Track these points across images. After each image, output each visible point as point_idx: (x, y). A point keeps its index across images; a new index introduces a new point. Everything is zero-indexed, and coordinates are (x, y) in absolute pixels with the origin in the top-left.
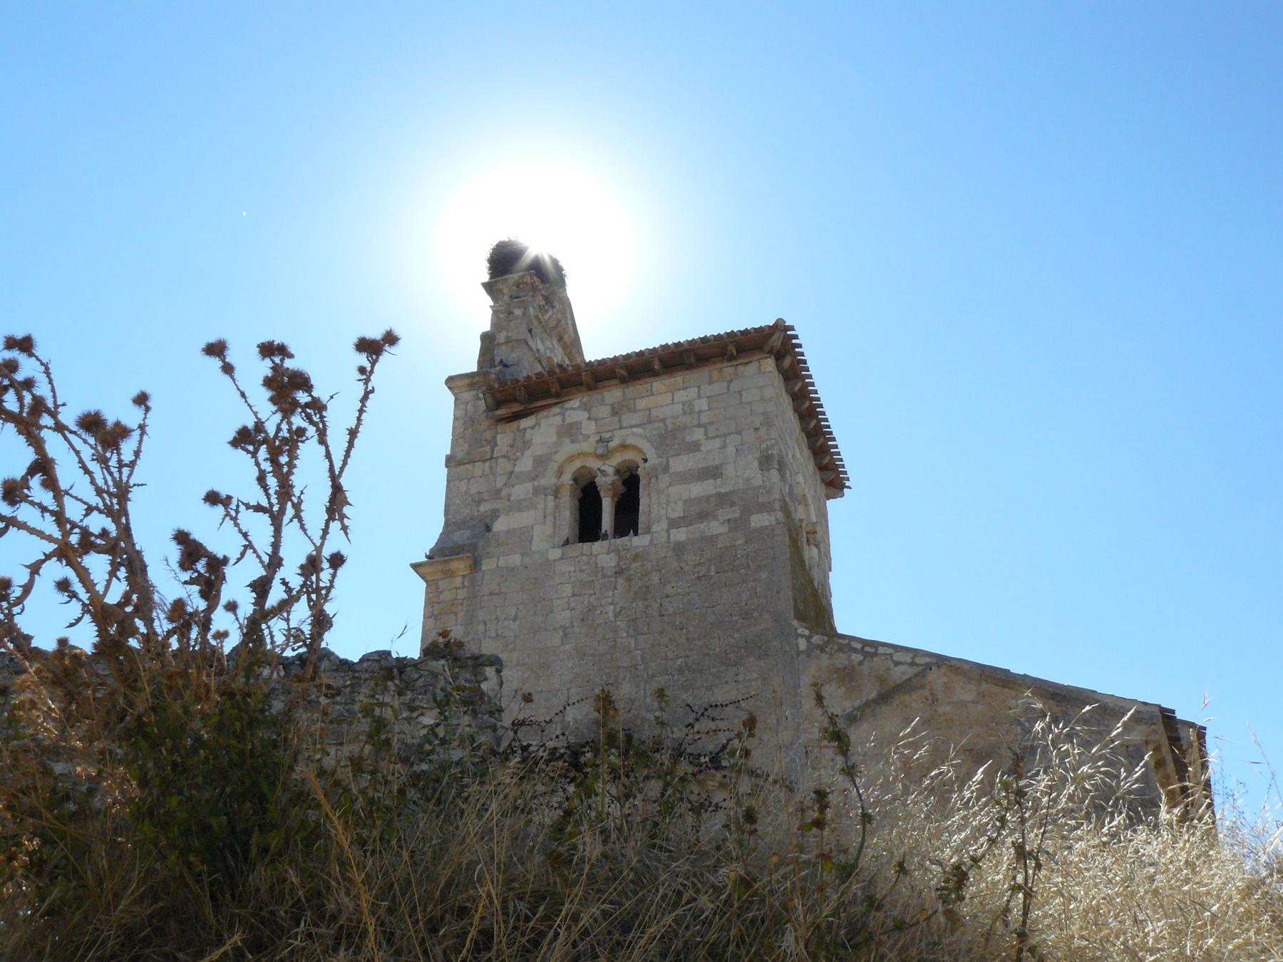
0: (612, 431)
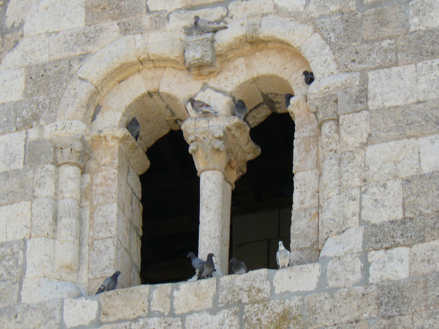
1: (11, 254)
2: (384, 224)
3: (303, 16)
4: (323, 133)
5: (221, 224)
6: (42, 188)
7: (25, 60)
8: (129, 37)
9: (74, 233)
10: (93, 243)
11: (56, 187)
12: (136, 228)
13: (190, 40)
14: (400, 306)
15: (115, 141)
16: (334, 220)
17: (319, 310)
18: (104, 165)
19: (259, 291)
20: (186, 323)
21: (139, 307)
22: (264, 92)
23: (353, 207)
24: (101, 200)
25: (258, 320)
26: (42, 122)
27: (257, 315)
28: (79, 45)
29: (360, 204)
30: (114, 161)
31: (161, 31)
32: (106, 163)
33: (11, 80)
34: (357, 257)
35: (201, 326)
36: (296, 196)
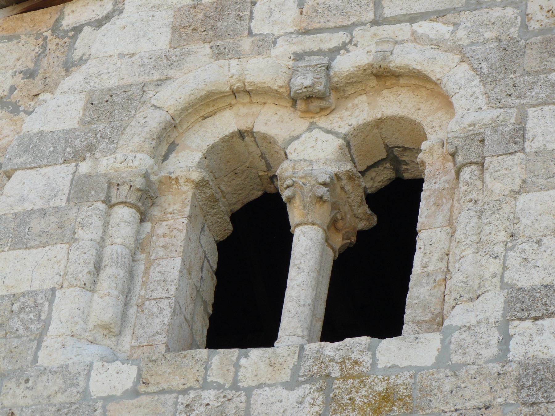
0: (348, 28)
1: (33, 305)
2: (534, 289)
3: (449, 43)
4: (461, 179)
5: (315, 292)
6: (86, 230)
7: (88, 83)
8: (222, 62)
9: (120, 286)
10: (143, 304)
11: (105, 231)
12: (204, 302)
13: (300, 65)
14: (548, 390)
15: (189, 185)
16: (466, 283)
17: (436, 391)
18: (171, 214)
19: (356, 363)
20: (252, 399)
21: (191, 377)
22: (388, 144)
23: (494, 266)
24: (161, 253)
25: (350, 399)
26: (98, 154)
27: (350, 393)
28: (158, 69)
29: (504, 264)
30: (185, 209)
31: (264, 56)
32: (174, 210)
33: (67, 105)
34: (495, 327)
35: (272, 403)
36: (418, 259)
